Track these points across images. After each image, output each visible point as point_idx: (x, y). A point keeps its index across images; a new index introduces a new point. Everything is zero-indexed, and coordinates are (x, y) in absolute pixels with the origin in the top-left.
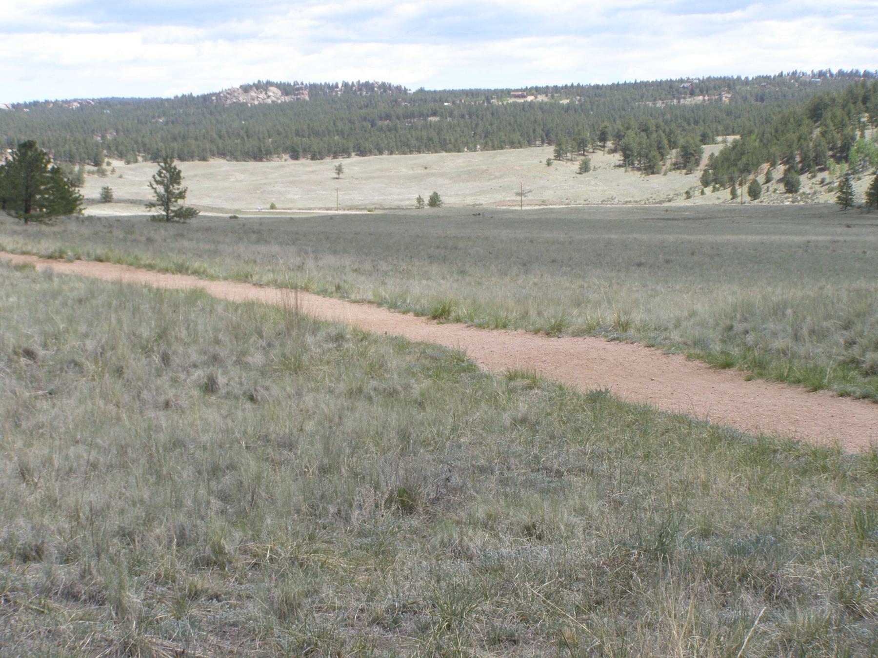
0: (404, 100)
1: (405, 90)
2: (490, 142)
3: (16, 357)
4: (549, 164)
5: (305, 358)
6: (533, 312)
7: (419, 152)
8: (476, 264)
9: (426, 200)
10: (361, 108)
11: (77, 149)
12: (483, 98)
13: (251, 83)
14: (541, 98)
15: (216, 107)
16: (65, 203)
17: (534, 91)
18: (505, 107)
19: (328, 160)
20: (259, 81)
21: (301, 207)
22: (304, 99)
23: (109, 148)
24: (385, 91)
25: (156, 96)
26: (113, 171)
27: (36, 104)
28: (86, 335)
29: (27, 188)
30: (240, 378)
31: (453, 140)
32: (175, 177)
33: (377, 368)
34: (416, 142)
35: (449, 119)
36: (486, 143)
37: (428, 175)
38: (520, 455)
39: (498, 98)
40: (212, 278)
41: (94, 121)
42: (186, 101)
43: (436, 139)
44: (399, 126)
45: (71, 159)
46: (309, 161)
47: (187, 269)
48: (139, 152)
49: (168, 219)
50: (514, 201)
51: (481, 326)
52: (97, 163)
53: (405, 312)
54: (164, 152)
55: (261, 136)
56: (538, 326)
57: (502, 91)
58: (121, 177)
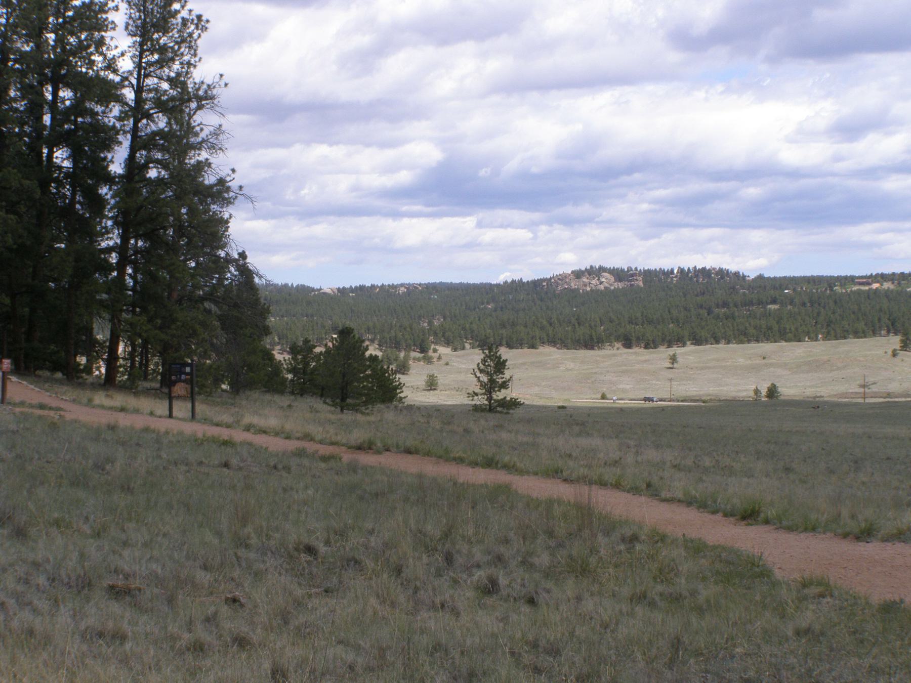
0: (742, 287)
1: (744, 277)
2: (832, 332)
3: (296, 554)
4: (894, 354)
5: (593, 560)
6: (845, 513)
7: (757, 341)
8: (805, 461)
9: (764, 392)
10: (697, 296)
11: (403, 335)
12: (826, 285)
13: (583, 269)
14: (887, 285)
15: (546, 293)
16: (387, 392)
17: (879, 278)
18: (849, 295)
19: (662, 349)
20: (591, 267)
21: (634, 397)
22: (638, 286)
23: (436, 334)
24: (722, 278)
25: (485, 280)
26: (439, 358)
27: (362, 288)
28: (371, 532)
29: (344, 376)
30: (523, 579)
31: (793, 329)
32: (500, 366)
33: (665, 573)
34: (754, 331)
35: (789, 307)
36: (828, 333)
37: (766, 365)
38: (793, 668)
39: (841, 286)
40: (521, 472)
41: (421, 307)
42: (516, 286)
43: (776, 327)
44: (737, 314)
45: (397, 346)
46: (642, 350)
47: (497, 463)
48: (467, 338)
49: (491, 409)
50: (856, 393)
51: (790, 529)
52: (423, 350)
53: (714, 512)
54: (492, 339)
55: (593, 324)
56: (848, 529)
57: (846, 278)
58: (447, 364)
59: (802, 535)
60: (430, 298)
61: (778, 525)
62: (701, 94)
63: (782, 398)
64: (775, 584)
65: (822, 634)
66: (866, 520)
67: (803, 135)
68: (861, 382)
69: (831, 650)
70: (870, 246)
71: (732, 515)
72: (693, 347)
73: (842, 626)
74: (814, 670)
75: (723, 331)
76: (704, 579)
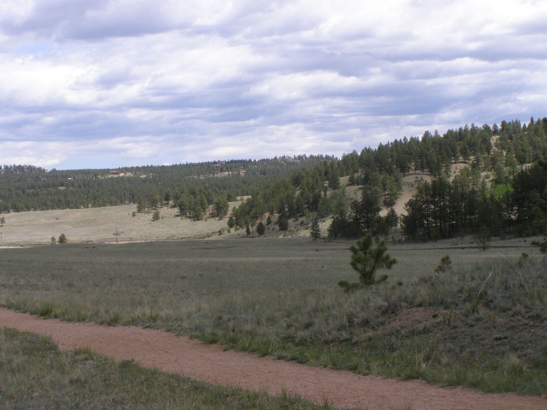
0: (43, 177)
1: (44, 170)
2: (97, 202)
4: (134, 215)
6: (102, 310)
7: (53, 209)
9: (57, 239)
12: (92, 174)
14: (129, 174)
18: (106, 180)
24: (31, 171)
25: (279, 155)
34: (51, 203)
35: (71, 188)
44: (40, 193)
50: (112, 238)
51: (69, 320)
53: (24, 312)
57: (104, 170)
59: (77, 324)
60: (474, 154)
61: (63, 318)
62: (19, 61)
63: (68, 242)
64: (58, 354)
65: (86, 381)
66: (114, 314)
67: (79, 86)
68: (115, 232)
69: (91, 391)
70: (119, 151)
71: (35, 313)
72: (14, 213)
73: (98, 376)
74: (79, 404)
75: (32, 203)
76: (16, 352)
